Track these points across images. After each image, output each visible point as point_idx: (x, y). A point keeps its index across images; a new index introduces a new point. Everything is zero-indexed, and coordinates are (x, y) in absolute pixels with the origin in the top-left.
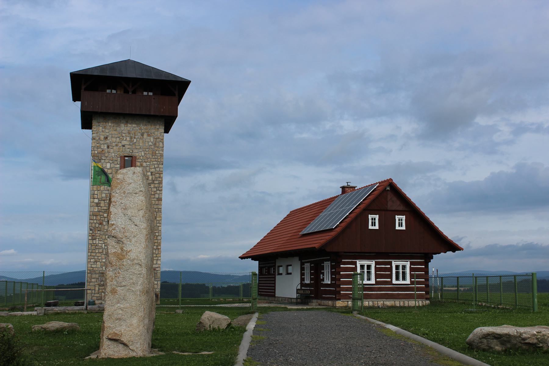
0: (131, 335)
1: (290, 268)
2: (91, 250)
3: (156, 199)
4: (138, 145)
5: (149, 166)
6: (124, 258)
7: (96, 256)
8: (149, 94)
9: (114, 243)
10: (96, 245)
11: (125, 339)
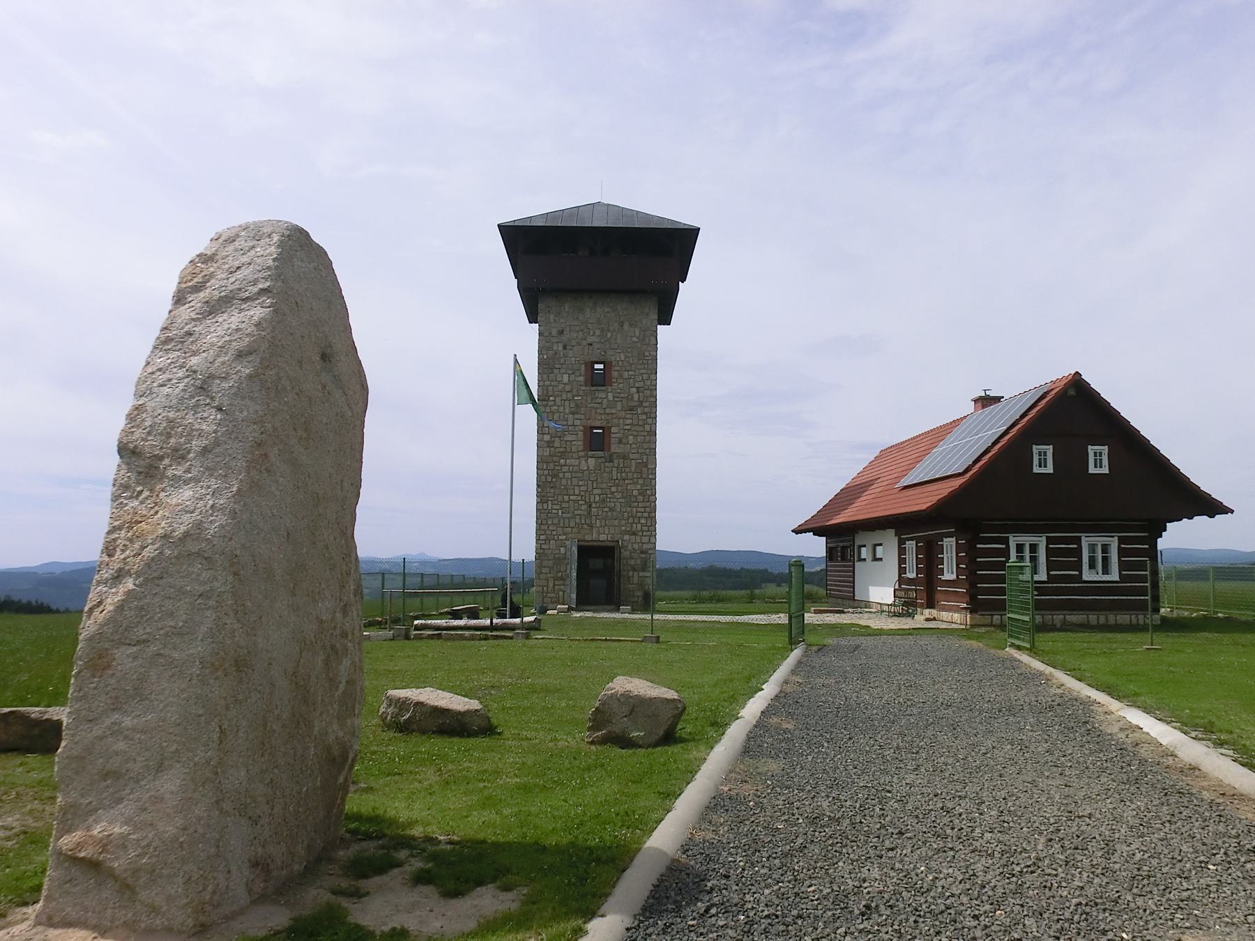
1: (878, 548)
3: (646, 434)
5: (633, 377)
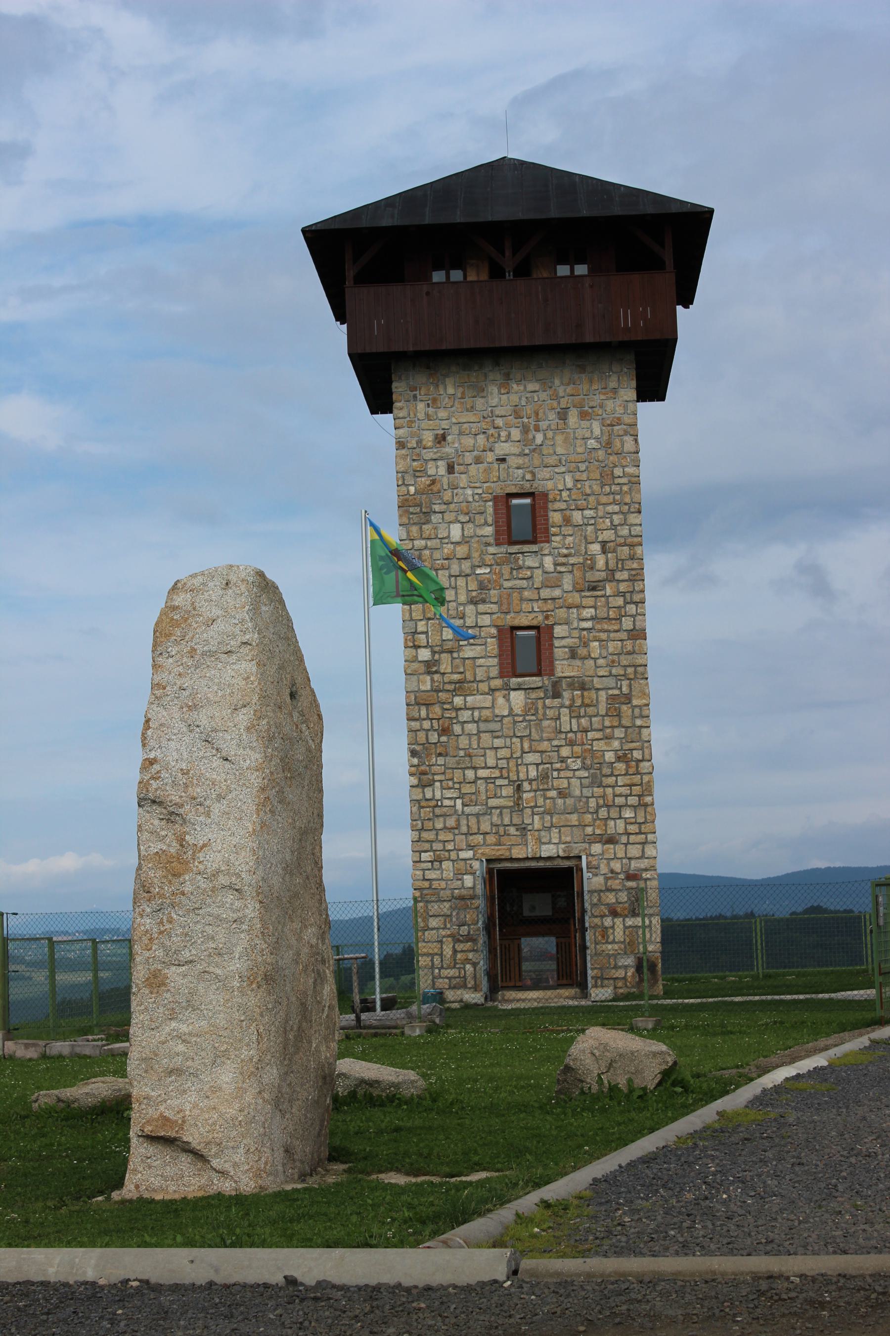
0: (214, 1124)
2: (419, 823)
3: (624, 635)
4: (551, 451)
5: (592, 521)
6: (188, 870)
7: (437, 840)
8: (577, 273)
9: (156, 822)
10: (433, 803)
11: (196, 1136)
